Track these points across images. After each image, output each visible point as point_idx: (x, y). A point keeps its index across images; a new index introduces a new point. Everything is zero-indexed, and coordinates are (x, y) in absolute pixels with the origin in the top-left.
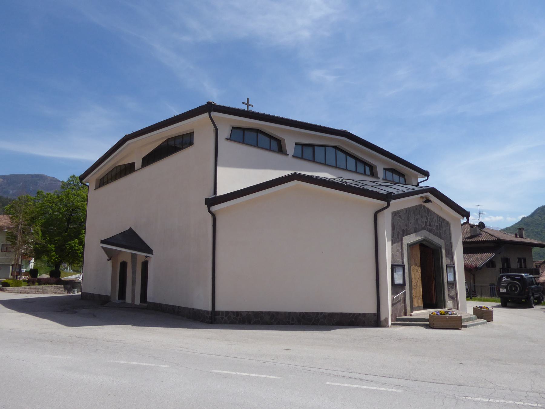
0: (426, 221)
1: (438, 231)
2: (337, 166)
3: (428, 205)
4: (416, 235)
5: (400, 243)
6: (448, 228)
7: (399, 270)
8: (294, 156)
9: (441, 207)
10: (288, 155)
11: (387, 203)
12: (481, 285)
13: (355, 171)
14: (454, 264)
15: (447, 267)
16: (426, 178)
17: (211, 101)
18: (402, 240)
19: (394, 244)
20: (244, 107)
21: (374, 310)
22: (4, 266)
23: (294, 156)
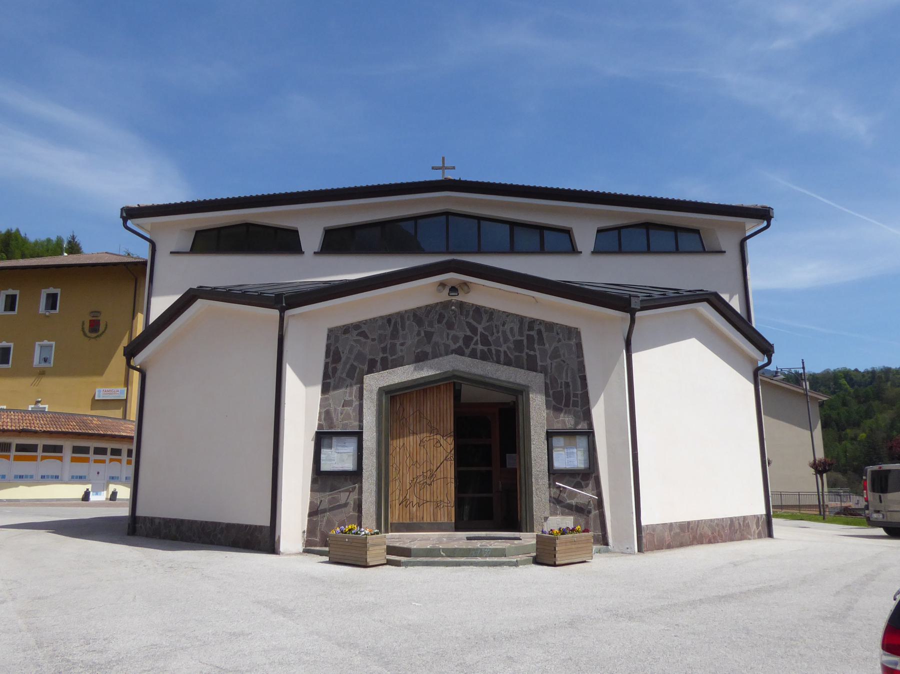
0: (469, 333)
1: (527, 354)
2: (706, 250)
3: (461, 297)
4: (415, 369)
5: (355, 388)
6: (573, 342)
7: (345, 443)
8: (596, 252)
9: (533, 297)
10: (581, 252)
11: (278, 311)
12: (799, 492)
13: (703, 250)
14: (591, 425)
15: (550, 435)
16: (765, 223)
17: (122, 207)
18: (361, 382)
19: (336, 388)
20: (437, 176)
21: (266, 522)
22: (579, 673)
23: (596, 252)
